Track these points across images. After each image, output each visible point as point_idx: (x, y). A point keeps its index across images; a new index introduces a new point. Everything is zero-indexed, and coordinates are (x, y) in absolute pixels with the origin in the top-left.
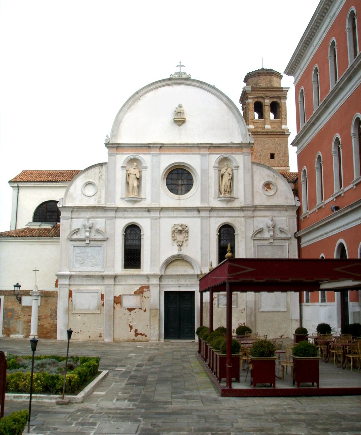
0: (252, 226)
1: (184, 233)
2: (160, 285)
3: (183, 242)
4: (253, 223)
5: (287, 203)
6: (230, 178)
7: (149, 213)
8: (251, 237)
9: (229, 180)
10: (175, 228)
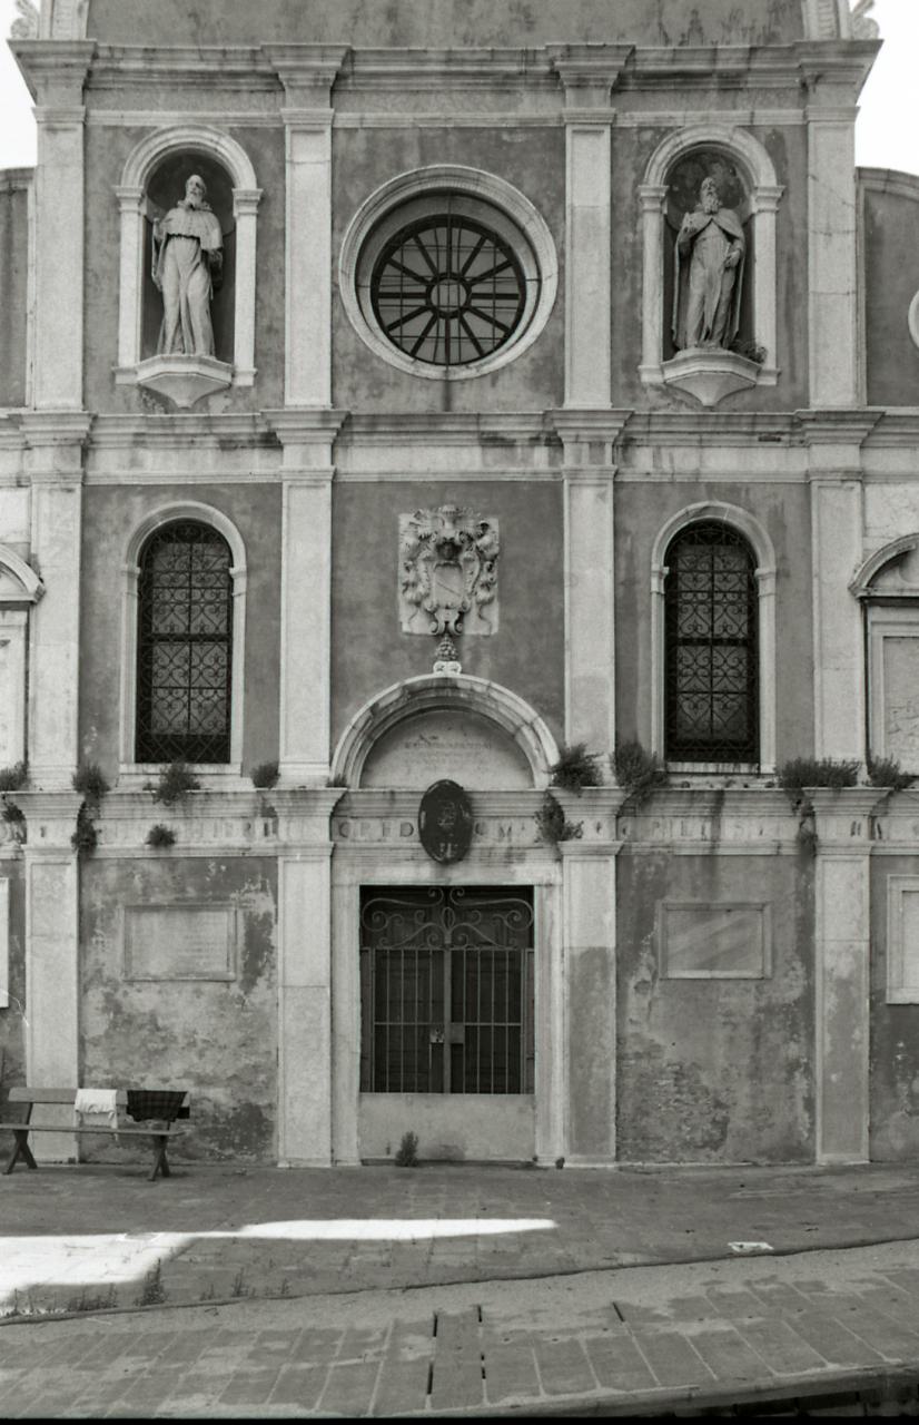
0: (857, 526)
1: (468, 561)
2: (334, 848)
3: (462, 615)
4: (863, 513)
5: (108, 219)
6: (735, 254)
7: (276, 454)
8: (852, 589)
9: (727, 269)
10: (421, 531)
